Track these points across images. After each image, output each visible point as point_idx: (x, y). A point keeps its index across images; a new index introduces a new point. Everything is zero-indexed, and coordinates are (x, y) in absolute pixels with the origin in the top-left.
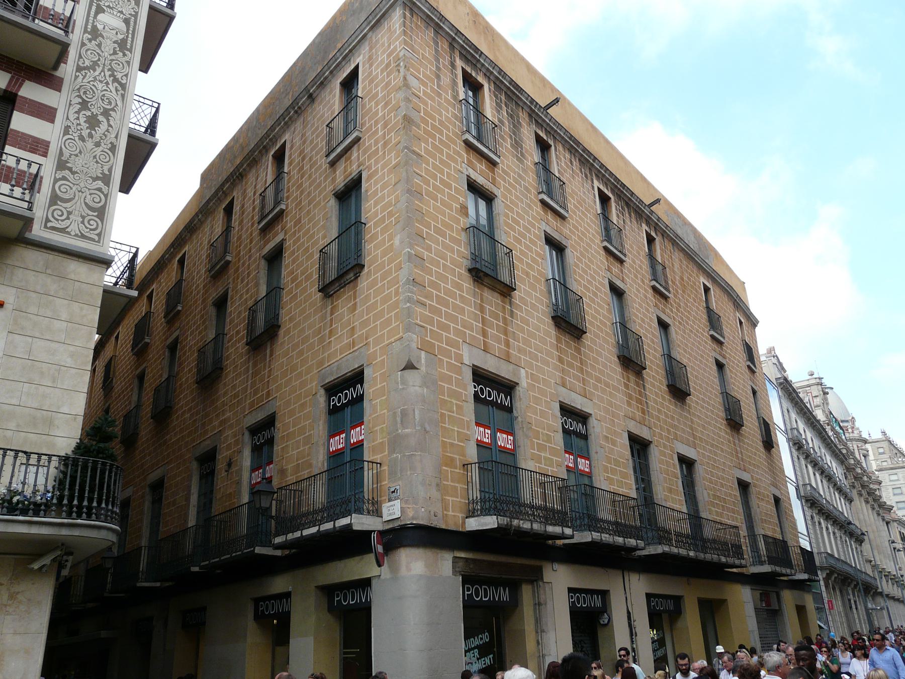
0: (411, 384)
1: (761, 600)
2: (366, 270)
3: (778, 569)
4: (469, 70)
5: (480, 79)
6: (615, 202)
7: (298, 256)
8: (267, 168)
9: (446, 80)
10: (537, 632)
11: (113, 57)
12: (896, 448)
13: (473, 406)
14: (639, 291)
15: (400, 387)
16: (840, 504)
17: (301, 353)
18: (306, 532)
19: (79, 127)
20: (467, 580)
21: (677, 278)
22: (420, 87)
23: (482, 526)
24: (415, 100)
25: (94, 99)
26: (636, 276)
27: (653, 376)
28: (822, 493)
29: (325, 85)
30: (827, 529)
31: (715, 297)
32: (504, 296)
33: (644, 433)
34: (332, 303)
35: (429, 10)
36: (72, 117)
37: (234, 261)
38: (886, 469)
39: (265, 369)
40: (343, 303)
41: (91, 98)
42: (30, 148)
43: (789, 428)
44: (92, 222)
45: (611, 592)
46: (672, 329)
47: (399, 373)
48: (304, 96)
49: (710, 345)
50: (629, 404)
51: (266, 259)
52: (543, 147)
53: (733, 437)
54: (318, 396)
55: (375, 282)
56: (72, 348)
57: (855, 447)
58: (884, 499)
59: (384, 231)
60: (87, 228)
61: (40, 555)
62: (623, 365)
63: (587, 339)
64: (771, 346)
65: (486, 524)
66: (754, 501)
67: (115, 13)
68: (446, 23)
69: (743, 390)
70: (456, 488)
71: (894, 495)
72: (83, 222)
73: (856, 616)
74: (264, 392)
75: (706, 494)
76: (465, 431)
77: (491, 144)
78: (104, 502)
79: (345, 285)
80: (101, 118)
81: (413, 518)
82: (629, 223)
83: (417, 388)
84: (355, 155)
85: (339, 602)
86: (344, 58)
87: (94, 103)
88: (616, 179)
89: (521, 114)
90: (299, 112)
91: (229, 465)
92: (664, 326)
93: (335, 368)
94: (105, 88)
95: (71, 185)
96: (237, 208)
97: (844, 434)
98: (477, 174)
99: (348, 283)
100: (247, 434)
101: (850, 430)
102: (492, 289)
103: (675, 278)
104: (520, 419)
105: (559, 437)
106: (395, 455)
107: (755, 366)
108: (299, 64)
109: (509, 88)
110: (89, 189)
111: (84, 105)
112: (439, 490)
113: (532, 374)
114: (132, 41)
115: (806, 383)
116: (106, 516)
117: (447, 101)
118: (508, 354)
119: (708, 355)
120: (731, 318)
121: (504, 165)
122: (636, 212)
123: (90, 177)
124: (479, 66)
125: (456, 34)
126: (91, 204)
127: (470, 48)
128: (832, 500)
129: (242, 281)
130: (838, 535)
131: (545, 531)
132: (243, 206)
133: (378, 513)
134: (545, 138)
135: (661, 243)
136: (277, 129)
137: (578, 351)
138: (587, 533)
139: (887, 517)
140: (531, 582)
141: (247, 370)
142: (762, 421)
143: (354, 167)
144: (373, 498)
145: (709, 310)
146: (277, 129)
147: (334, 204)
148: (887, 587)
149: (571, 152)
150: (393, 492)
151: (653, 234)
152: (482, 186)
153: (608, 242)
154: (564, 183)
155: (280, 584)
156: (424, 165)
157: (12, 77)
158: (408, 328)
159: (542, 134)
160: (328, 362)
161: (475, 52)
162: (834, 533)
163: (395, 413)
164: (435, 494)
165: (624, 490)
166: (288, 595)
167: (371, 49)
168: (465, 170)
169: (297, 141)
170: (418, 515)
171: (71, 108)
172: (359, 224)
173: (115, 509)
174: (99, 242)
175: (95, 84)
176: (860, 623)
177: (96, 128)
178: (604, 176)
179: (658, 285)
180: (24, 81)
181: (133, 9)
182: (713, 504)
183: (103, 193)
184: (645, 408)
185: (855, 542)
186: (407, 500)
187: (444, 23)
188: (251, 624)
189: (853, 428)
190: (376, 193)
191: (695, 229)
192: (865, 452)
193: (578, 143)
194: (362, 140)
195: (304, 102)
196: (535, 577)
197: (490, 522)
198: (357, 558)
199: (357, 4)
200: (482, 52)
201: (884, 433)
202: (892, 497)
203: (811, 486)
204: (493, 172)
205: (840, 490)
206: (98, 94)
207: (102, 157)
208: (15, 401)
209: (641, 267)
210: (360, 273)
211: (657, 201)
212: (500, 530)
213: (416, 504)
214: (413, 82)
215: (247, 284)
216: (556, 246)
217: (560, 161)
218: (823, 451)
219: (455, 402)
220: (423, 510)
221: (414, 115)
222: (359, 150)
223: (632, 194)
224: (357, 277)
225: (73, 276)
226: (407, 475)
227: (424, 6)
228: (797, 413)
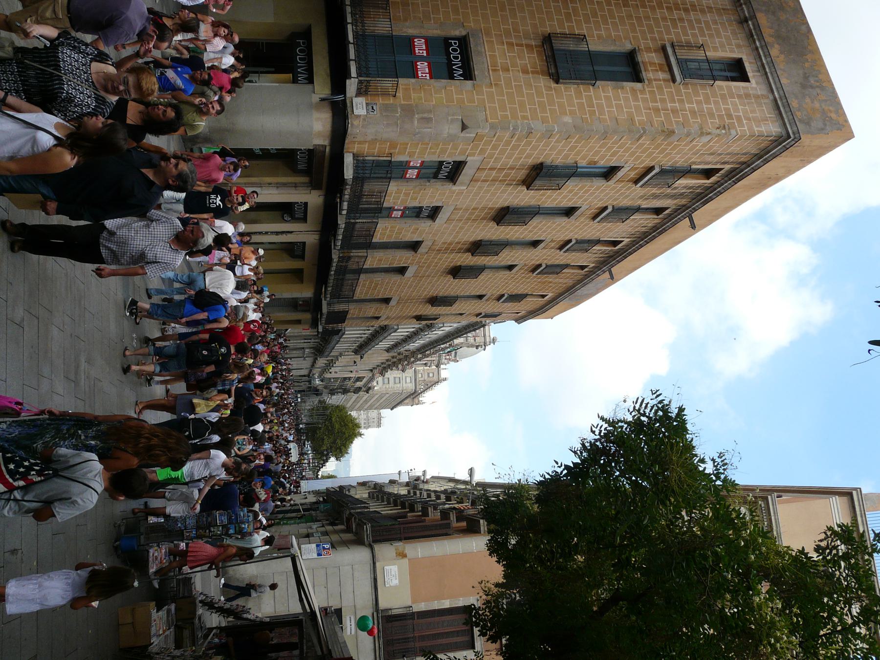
0: (451, 126)
2: (553, 85)
4: (722, 172)
5: (713, 179)
6: (612, 250)
9: (710, 158)
10: (277, 184)
12: (432, 386)
13: (436, 160)
15: (449, 118)
20: (311, 152)
23: (346, 166)
24: (689, 139)
29: (748, 39)
30: (365, 334)
33: (422, 249)
35: (773, 154)
40: (532, 59)
50: (444, 243)
52: (658, 211)
53: (423, 299)
54: (461, 29)
55: (539, 94)
57: (434, 359)
58: (389, 372)
59: (581, 105)
63: (493, 224)
65: (347, 169)
66: (375, 305)
68: (762, 164)
70: (375, 149)
71: (395, 378)
73: (299, 341)
76: (416, 156)
79: (547, 62)
81: (352, 125)
83: (447, 131)
84: (661, 75)
85: (299, 45)
88: (631, 254)
92: (510, 268)
101: (448, 357)
102: (527, 175)
104: (428, 184)
105: (416, 204)
106: (399, 110)
112: (372, 139)
113: (463, 193)
115: (487, 334)
119: (585, 200)
122: (605, 261)
127: (741, 176)
131: (344, 201)
133: (359, 94)
137: (484, 219)
139: (376, 371)
140: (311, 182)
154: (623, 222)
158: (492, 127)
161: (737, 178)
162: (361, 337)
163: (430, 111)
164: (369, 138)
170: (355, 128)
176: (293, 343)
179: (542, 268)
182: (371, 282)
185: (355, 349)
187: (762, 161)
189: (450, 359)
190: (617, 98)
192: (429, 365)
193: (660, 233)
194: (672, 84)
196: (314, 185)
197: (349, 173)
200: (736, 183)
201: (445, 379)
205: (396, 346)
211: (612, 277)
212: (342, 181)
214: (705, 139)
217: (649, 220)
218: (427, 339)
219: (438, 151)
221: (674, 138)
222: (664, 80)
223: (619, 262)
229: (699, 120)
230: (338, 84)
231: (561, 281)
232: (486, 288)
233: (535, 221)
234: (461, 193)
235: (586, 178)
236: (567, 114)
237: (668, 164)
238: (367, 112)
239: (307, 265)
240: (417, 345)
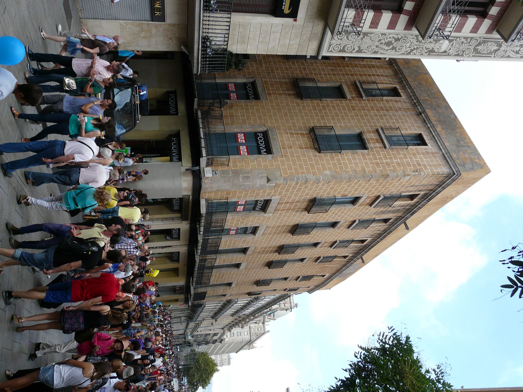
1: (179, 288)
2: (318, 154)
3: (192, 296)
5: (415, 200)
6: (361, 246)
8: (390, 84)
9: (411, 189)
10: (162, 218)
11: (424, 48)
12: (261, 336)
16: (230, 311)
17: (286, 115)
18: (200, 121)
19: (386, 39)
20: (181, 199)
23: (202, 206)
25: (401, 43)
30: (218, 306)
33: (249, 252)
36: (391, 36)
37: (344, 62)
38: (250, 330)
39: (282, 90)
40: (305, 141)
41: (401, 42)
42: (373, 22)
44: (337, 48)
45: (179, 241)
46: (301, 263)
47: (266, 175)
48: (421, 110)
50: (262, 248)
53: (251, 282)
55: (310, 160)
56: (277, 47)
57: (261, 319)
59: (334, 165)
60: (334, 46)
61: (186, 47)
63: (290, 235)
65: (202, 208)
67: (449, 47)
71: (237, 332)
72: (337, 45)
73: (178, 313)
75: (224, 272)
77: (381, 204)
78: (209, 63)
79: (313, 142)
80: (391, 46)
84: (378, 145)
86: (433, 136)
87: (399, 43)
88: (373, 247)
89: (400, 213)
90: (415, 106)
92: (302, 260)
93: (274, 137)
94: (407, 47)
95: (355, 39)
99: (314, 144)
100: (251, 80)
101: (269, 317)
104: (250, 214)
108: (443, 104)
109: (412, 210)
110: (354, 46)
111: (398, 40)
113: (270, 218)
114: (434, 55)
116: (203, 65)
118: (278, 210)
120: (310, 284)
123: (360, 45)
124: (422, 199)
125: (437, 193)
126: (346, 47)
127: (431, 197)
130: (215, 309)
132: (373, 67)
133: (208, 165)
134: (389, 222)
136: (409, 91)
137: (284, 232)
138: (201, 241)
139: (225, 329)
141: (284, 78)
143: (372, 145)
146: (409, 91)
147: (356, 132)
148: (192, 325)
149: (384, 230)
151: (347, 258)
154: (390, 206)
155: (182, 107)
157: (410, 11)
158: (285, 179)
159: (391, 221)
160: (278, 133)
162: (216, 308)
164: (215, 189)
166: (177, 114)
167: (433, 153)
169: (399, 105)
170: (206, 184)
171: (396, 35)
172: (341, 148)
173: (207, 71)
174: (328, 51)
175: (409, 43)
177: (385, 45)
178: (374, 242)
179: (321, 259)
180: (408, 16)
181: (452, 54)
183: (352, 50)
186: (212, 180)
188: (164, 90)
189: (270, 319)
190: (354, 159)
191: (354, 273)
192: (258, 323)
193: (389, 234)
194: (384, 149)
195: (418, 109)
196: (184, 218)
197: (203, 210)
198: (190, 154)
199: (462, 143)
200: (429, 202)
202: (236, 331)
203: (238, 301)
205: (237, 312)
206: (404, 45)
207: (371, 49)
208: (251, 30)
210: (317, 151)
213: (210, 184)
214: (407, 178)
218: (256, 307)
219: (254, 195)
220: (208, 186)
222: (380, 148)
223: (366, 252)
225: (310, 43)
226: (222, 179)
227: (449, 182)
229: (402, 168)
230: (196, 159)
231: (333, 266)
233: (314, 232)
234: (269, 218)
239: (181, 265)
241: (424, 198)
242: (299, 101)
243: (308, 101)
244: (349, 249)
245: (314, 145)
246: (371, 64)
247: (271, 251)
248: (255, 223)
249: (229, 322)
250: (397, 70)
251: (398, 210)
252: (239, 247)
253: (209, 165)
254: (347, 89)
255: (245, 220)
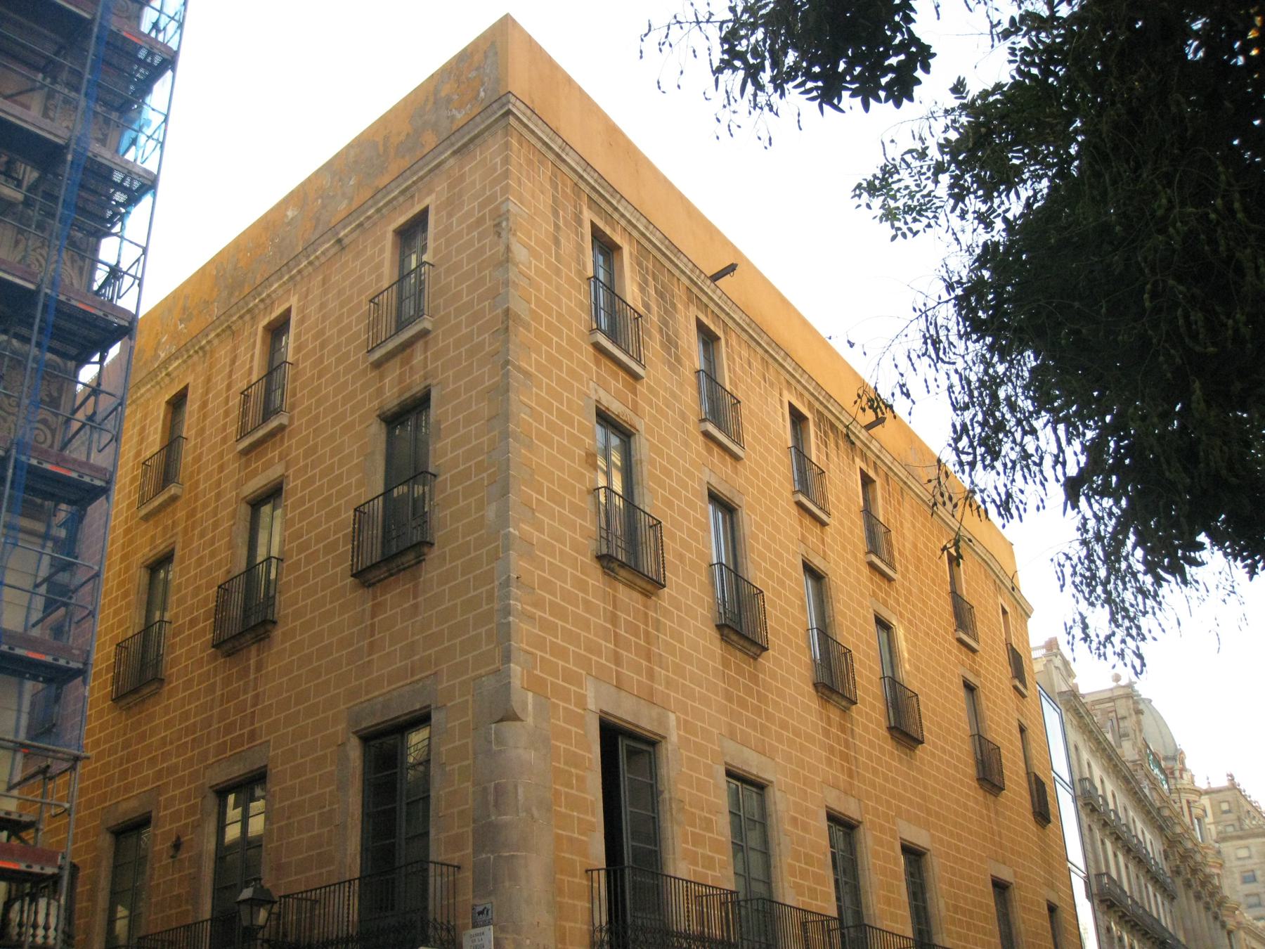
4: (601, 224)
5: (618, 239)
7: (311, 508)
9: (567, 245)
14: (848, 573)
21: (908, 545)
22: (531, 262)
26: (844, 548)
27: (867, 713)
28: (1126, 888)
31: (965, 574)
32: (646, 596)
33: (851, 809)
34: (374, 598)
40: (393, 597)
43: (1077, 778)
49: (956, 656)
50: (829, 762)
51: (248, 503)
62: (822, 698)
63: (767, 661)
64: (1052, 636)
69: (1005, 729)
74: (245, 731)
82: (836, 459)
84: (418, 358)
89: (676, 290)
90: (317, 263)
91: (177, 846)
96: (192, 406)
97: (1167, 782)
98: (610, 398)
102: (630, 587)
103: (904, 545)
106: (484, 856)
107: (1025, 686)
113: (686, 721)
117: (570, 281)
120: (989, 608)
121: (650, 379)
128: (1142, 898)
129: (202, 535)
135: (883, 488)
137: (754, 678)
142: (1033, 779)
143: (417, 377)
144: (448, 922)
145: (956, 596)
150: (481, 913)
151: (872, 474)
152: (618, 416)
153: (803, 493)
154: (739, 402)
156: (534, 389)
163: (485, 789)
165: (819, 903)
168: (593, 392)
183: (49, 428)
184: (853, 768)
194: (431, 336)
201: (1231, 777)
204: (634, 392)
205: (1155, 879)
209: (851, 532)
215: (212, 541)
216: (725, 506)
218: (1131, 813)
220: (528, 942)
222: (426, 350)
224: (420, 562)
228: (1092, 751)
229: (487, 272)
231: (907, 525)
232: (943, 676)
233: (755, 574)
234: (686, 726)
235: (634, 476)
236: (483, 515)
237: (585, 320)
238: (489, 924)
240: (1148, 836)
241: (610, 210)
242: (280, 631)
243: (280, 602)
244: (831, 466)
245: (409, 567)
246: (199, 412)
247: (843, 729)
248: (711, 777)
249: (1211, 918)
250: (219, 330)
251: (661, 295)
252: (991, 902)
253: (454, 940)
254: (259, 477)
255: (693, 814)
